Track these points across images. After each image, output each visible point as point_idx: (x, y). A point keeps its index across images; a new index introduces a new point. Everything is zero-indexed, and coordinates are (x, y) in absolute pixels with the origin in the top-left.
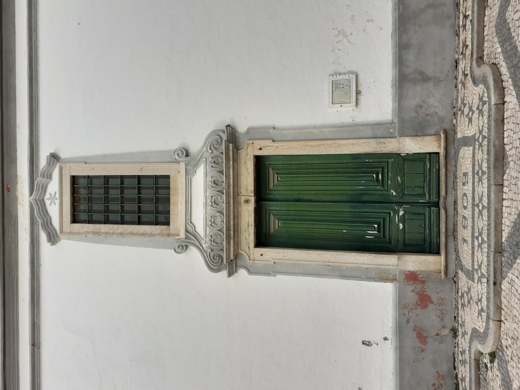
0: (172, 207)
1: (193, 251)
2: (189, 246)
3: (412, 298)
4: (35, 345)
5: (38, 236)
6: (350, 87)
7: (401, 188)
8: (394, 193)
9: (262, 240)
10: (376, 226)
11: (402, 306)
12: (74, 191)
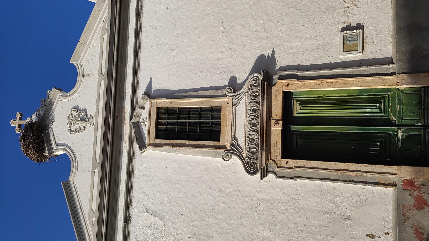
0: (222, 128)
1: (235, 160)
2: (233, 156)
3: (410, 201)
4: (127, 220)
5: (133, 145)
6: (358, 40)
7: (399, 115)
8: (394, 119)
9: (286, 154)
10: (379, 144)
11: (401, 211)
12: (158, 118)
